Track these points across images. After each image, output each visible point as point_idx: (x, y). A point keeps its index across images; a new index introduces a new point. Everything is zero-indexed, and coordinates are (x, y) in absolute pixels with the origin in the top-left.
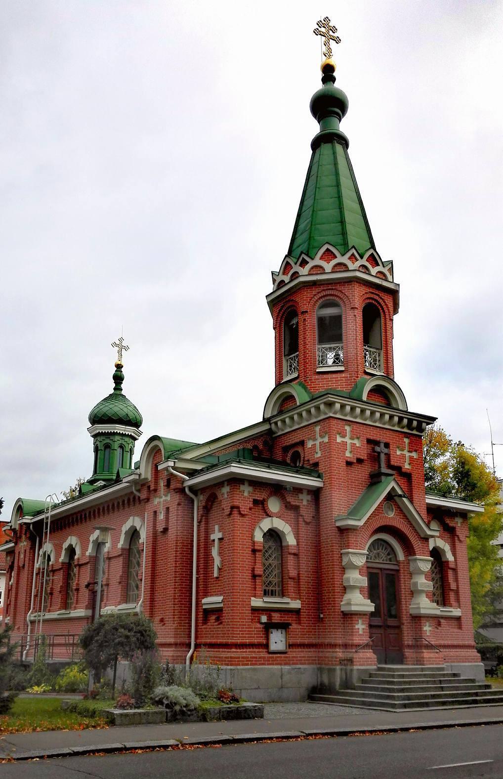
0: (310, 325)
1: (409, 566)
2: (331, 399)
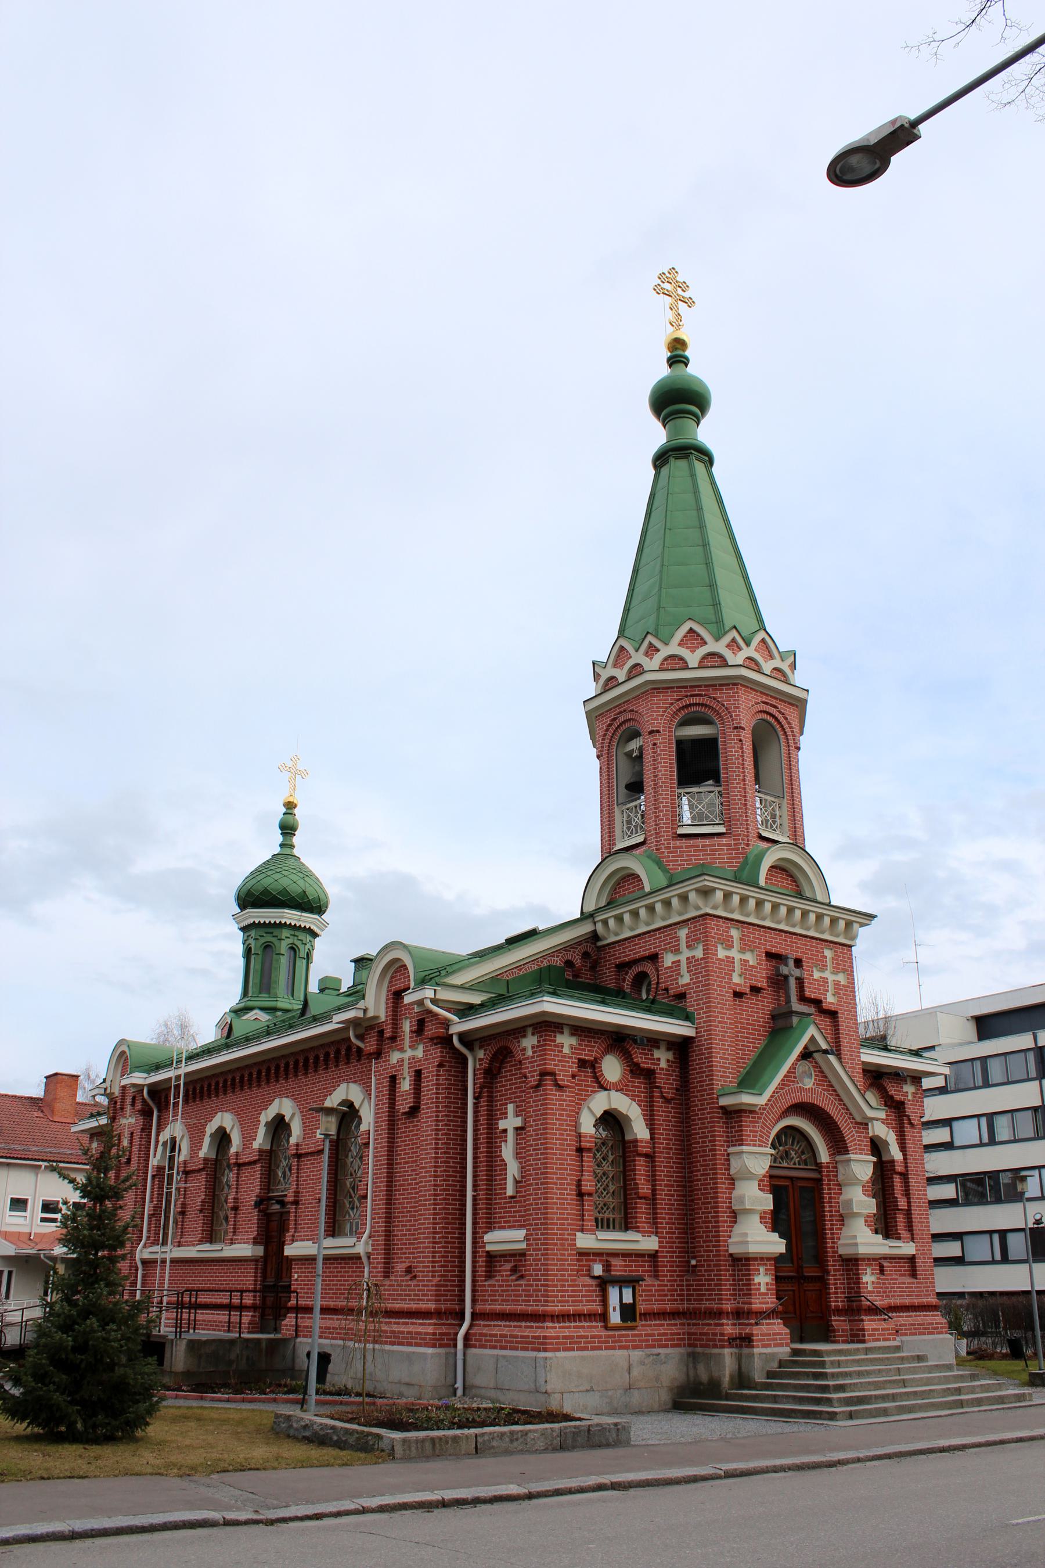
0: (664, 755)
1: (837, 1172)
2: (709, 882)
